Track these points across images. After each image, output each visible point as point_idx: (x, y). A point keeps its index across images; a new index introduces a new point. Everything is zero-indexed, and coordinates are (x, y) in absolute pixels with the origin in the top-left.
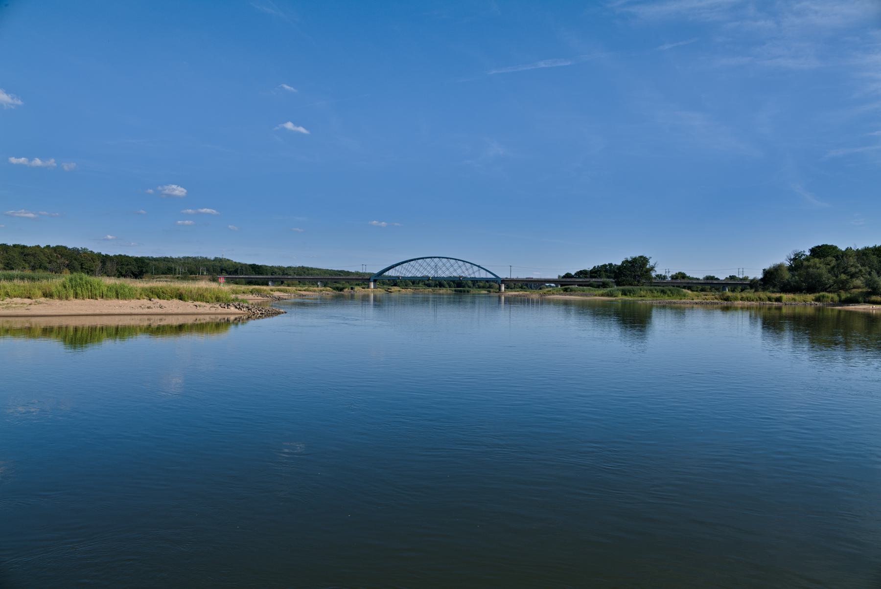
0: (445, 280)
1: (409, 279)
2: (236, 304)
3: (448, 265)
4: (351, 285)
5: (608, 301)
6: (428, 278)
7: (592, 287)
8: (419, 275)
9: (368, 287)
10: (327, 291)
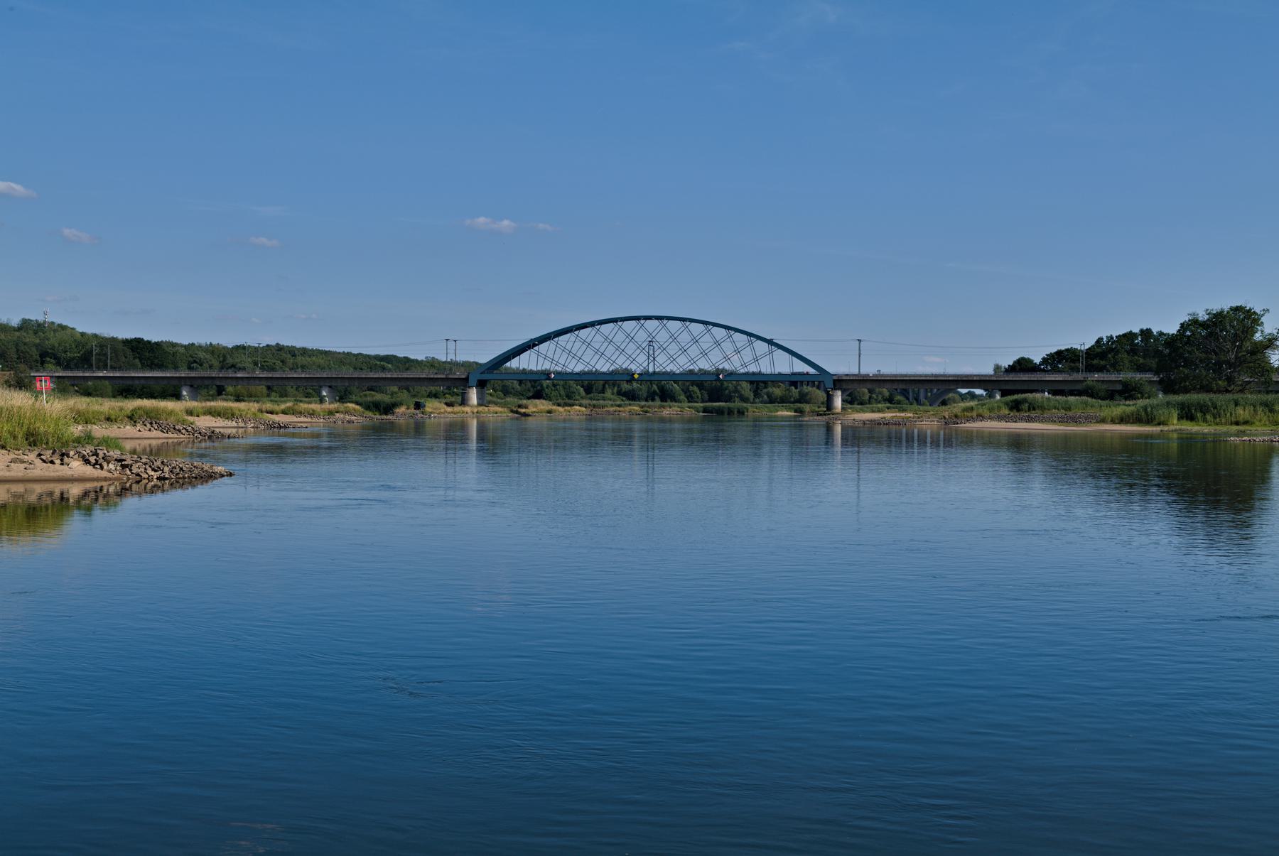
0: (675, 382)
1: (578, 377)
2: (87, 450)
3: (685, 338)
4: (414, 396)
5: (1140, 436)
6: (629, 376)
7: (1092, 396)
8: (603, 366)
9: (464, 402)
10: (347, 412)
